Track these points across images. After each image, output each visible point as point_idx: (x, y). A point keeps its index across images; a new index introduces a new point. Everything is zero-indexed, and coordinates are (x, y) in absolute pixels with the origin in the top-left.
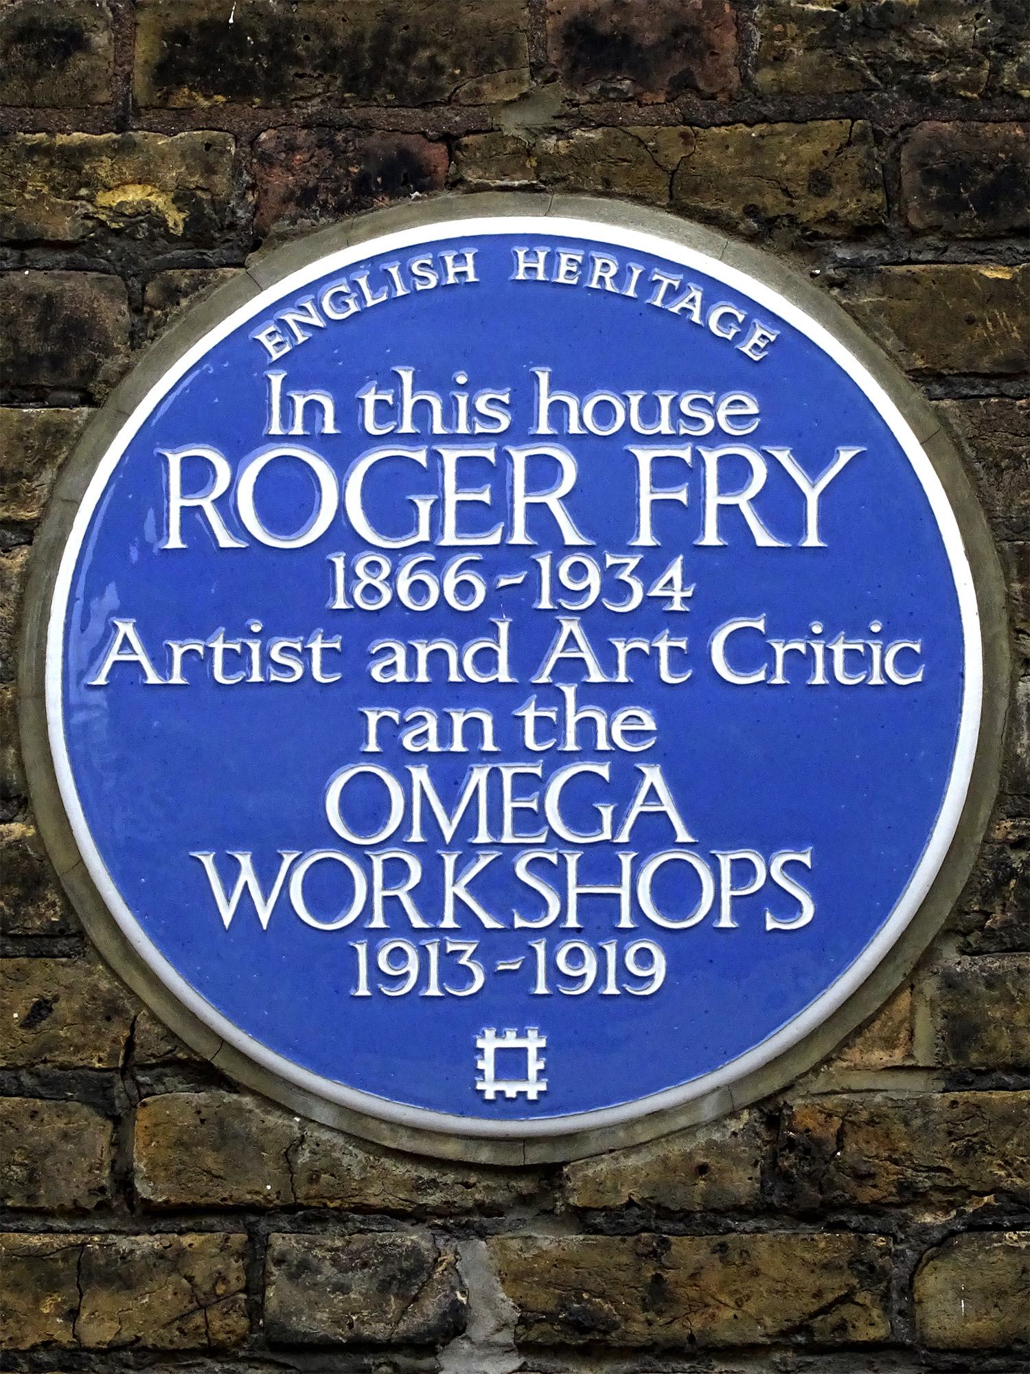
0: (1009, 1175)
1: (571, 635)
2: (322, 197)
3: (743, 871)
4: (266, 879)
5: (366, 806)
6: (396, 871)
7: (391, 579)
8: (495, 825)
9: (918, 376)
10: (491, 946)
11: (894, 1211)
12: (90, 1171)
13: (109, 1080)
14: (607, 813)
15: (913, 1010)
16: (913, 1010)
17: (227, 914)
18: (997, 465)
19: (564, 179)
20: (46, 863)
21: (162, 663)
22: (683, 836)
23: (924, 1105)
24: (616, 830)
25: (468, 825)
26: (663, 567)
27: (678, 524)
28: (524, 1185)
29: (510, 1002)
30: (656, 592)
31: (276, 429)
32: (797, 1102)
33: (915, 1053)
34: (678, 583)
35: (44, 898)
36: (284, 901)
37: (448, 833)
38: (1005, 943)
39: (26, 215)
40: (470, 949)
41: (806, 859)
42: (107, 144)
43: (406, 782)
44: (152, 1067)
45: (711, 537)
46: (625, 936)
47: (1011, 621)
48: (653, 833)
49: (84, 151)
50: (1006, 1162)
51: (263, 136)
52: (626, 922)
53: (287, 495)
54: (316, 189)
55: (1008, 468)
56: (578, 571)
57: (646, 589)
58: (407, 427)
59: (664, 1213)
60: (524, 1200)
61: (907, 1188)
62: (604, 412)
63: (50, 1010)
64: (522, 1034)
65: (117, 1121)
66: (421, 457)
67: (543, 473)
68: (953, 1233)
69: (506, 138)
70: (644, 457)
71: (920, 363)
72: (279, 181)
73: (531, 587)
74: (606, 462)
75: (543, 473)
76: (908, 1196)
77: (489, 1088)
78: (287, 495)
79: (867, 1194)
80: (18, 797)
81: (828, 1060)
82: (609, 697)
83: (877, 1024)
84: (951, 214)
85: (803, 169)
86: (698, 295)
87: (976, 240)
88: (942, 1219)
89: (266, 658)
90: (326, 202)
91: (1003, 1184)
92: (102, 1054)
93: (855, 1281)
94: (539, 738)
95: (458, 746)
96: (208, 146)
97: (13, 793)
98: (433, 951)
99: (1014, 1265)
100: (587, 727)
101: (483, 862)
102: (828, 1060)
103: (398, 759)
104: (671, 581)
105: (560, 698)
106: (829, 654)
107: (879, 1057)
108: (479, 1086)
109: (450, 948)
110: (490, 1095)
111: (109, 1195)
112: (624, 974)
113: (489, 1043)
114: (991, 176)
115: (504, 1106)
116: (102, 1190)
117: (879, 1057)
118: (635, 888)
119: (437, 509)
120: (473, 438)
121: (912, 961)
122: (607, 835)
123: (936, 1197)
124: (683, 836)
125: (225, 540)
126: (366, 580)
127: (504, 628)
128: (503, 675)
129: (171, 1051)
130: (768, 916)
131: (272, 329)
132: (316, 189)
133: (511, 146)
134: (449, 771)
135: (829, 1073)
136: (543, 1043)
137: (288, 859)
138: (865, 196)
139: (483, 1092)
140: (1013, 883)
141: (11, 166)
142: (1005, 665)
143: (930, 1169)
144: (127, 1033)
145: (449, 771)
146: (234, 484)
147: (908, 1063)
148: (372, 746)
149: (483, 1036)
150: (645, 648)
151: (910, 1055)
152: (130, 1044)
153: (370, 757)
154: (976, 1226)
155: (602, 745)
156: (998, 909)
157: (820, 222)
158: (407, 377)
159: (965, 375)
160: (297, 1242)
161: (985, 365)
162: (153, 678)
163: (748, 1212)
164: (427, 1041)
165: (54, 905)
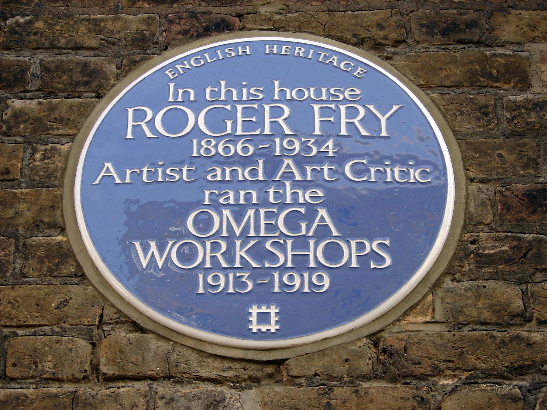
0: (480, 363)
1: (288, 164)
2: (191, 33)
3: (360, 247)
4: (161, 250)
5: (204, 223)
6: (215, 247)
7: (216, 146)
8: (257, 229)
9: (421, 86)
10: (255, 274)
11: (430, 379)
12: (81, 363)
13: (92, 329)
14: (303, 226)
15: (433, 301)
16: (433, 301)
17: (144, 264)
18: (455, 114)
19: (283, 27)
20: (71, 250)
21: (123, 176)
22: (335, 233)
23: (440, 335)
24: (308, 229)
25: (246, 229)
26: (325, 142)
27: (330, 129)
28: (269, 369)
29: (263, 295)
30: (322, 150)
31: (171, 99)
32: (385, 335)
33: (436, 317)
34: (331, 147)
35: (68, 263)
36: (169, 258)
37: (238, 233)
38: (471, 277)
39: (78, 39)
40: (246, 275)
41: (387, 243)
42: (111, 18)
43: (221, 215)
44: (110, 324)
45: (343, 132)
46: (312, 270)
47: (464, 166)
48: (323, 232)
49: (102, 20)
50: (478, 358)
51: (170, 15)
52: (312, 264)
53: (175, 120)
54: (189, 31)
55: (459, 115)
56: (291, 143)
57: (318, 149)
58: (223, 98)
59: (331, 377)
60: (270, 376)
61: (436, 369)
62: (300, 93)
63: (68, 303)
64: (268, 307)
65: (93, 345)
66: (228, 107)
67: (276, 112)
68: (457, 386)
69: (262, 15)
70: (316, 107)
71: (422, 82)
72: (176, 28)
73: (272, 148)
74: (302, 109)
75: (276, 112)
76: (437, 372)
77: (254, 328)
78: (175, 120)
79: (418, 370)
80: (61, 227)
81: (399, 320)
82: (304, 184)
83: (419, 307)
84: (431, 36)
85: (374, 23)
86: (336, 58)
87: (441, 45)
88: (450, 382)
89: (164, 173)
90: (193, 34)
91: (478, 366)
92: (89, 319)
93: (416, 404)
94: (275, 198)
95: (242, 202)
96: (149, 18)
97: (59, 226)
98: (231, 276)
99: (485, 397)
100: (295, 195)
101: (252, 243)
102: (399, 320)
103: (218, 208)
104: (328, 146)
105: (284, 186)
106: (392, 171)
107: (421, 319)
108: (250, 327)
109: (238, 275)
110: (255, 331)
111: (88, 373)
112: (311, 284)
113: (254, 310)
114: (446, 25)
115: (261, 335)
116: (86, 371)
117: (421, 319)
118: (316, 253)
119: (235, 123)
120: (248, 101)
121: (431, 284)
122: (304, 233)
123: (449, 372)
124: (335, 233)
125: (149, 135)
126: (206, 146)
127: (261, 162)
128: (261, 177)
129: (119, 318)
130: (372, 263)
131: (171, 69)
132: (189, 31)
133: (263, 17)
134: (239, 212)
135: (399, 325)
136: (277, 311)
137: (171, 243)
138: (398, 31)
139: (252, 329)
140: (472, 255)
141: (73, 25)
142: (463, 181)
143: (445, 361)
144: (100, 312)
145: (239, 212)
146: (153, 119)
147: (433, 321)
148: (207, 202)
149: (252, 308)
150: (318, 168)
151: (433, 317)
152: (101, 316)
153: (207, 206)
154: (468, 383)
155: (301, 201)
156: (467, 265)
157: (382, 39)
158: (223, 83)
159: (440, 86)
160: (170, 390)
161: (448, 83)
162: (118, 181)
163: (367, 378)
164: (228, 312)
165: (73, 265)
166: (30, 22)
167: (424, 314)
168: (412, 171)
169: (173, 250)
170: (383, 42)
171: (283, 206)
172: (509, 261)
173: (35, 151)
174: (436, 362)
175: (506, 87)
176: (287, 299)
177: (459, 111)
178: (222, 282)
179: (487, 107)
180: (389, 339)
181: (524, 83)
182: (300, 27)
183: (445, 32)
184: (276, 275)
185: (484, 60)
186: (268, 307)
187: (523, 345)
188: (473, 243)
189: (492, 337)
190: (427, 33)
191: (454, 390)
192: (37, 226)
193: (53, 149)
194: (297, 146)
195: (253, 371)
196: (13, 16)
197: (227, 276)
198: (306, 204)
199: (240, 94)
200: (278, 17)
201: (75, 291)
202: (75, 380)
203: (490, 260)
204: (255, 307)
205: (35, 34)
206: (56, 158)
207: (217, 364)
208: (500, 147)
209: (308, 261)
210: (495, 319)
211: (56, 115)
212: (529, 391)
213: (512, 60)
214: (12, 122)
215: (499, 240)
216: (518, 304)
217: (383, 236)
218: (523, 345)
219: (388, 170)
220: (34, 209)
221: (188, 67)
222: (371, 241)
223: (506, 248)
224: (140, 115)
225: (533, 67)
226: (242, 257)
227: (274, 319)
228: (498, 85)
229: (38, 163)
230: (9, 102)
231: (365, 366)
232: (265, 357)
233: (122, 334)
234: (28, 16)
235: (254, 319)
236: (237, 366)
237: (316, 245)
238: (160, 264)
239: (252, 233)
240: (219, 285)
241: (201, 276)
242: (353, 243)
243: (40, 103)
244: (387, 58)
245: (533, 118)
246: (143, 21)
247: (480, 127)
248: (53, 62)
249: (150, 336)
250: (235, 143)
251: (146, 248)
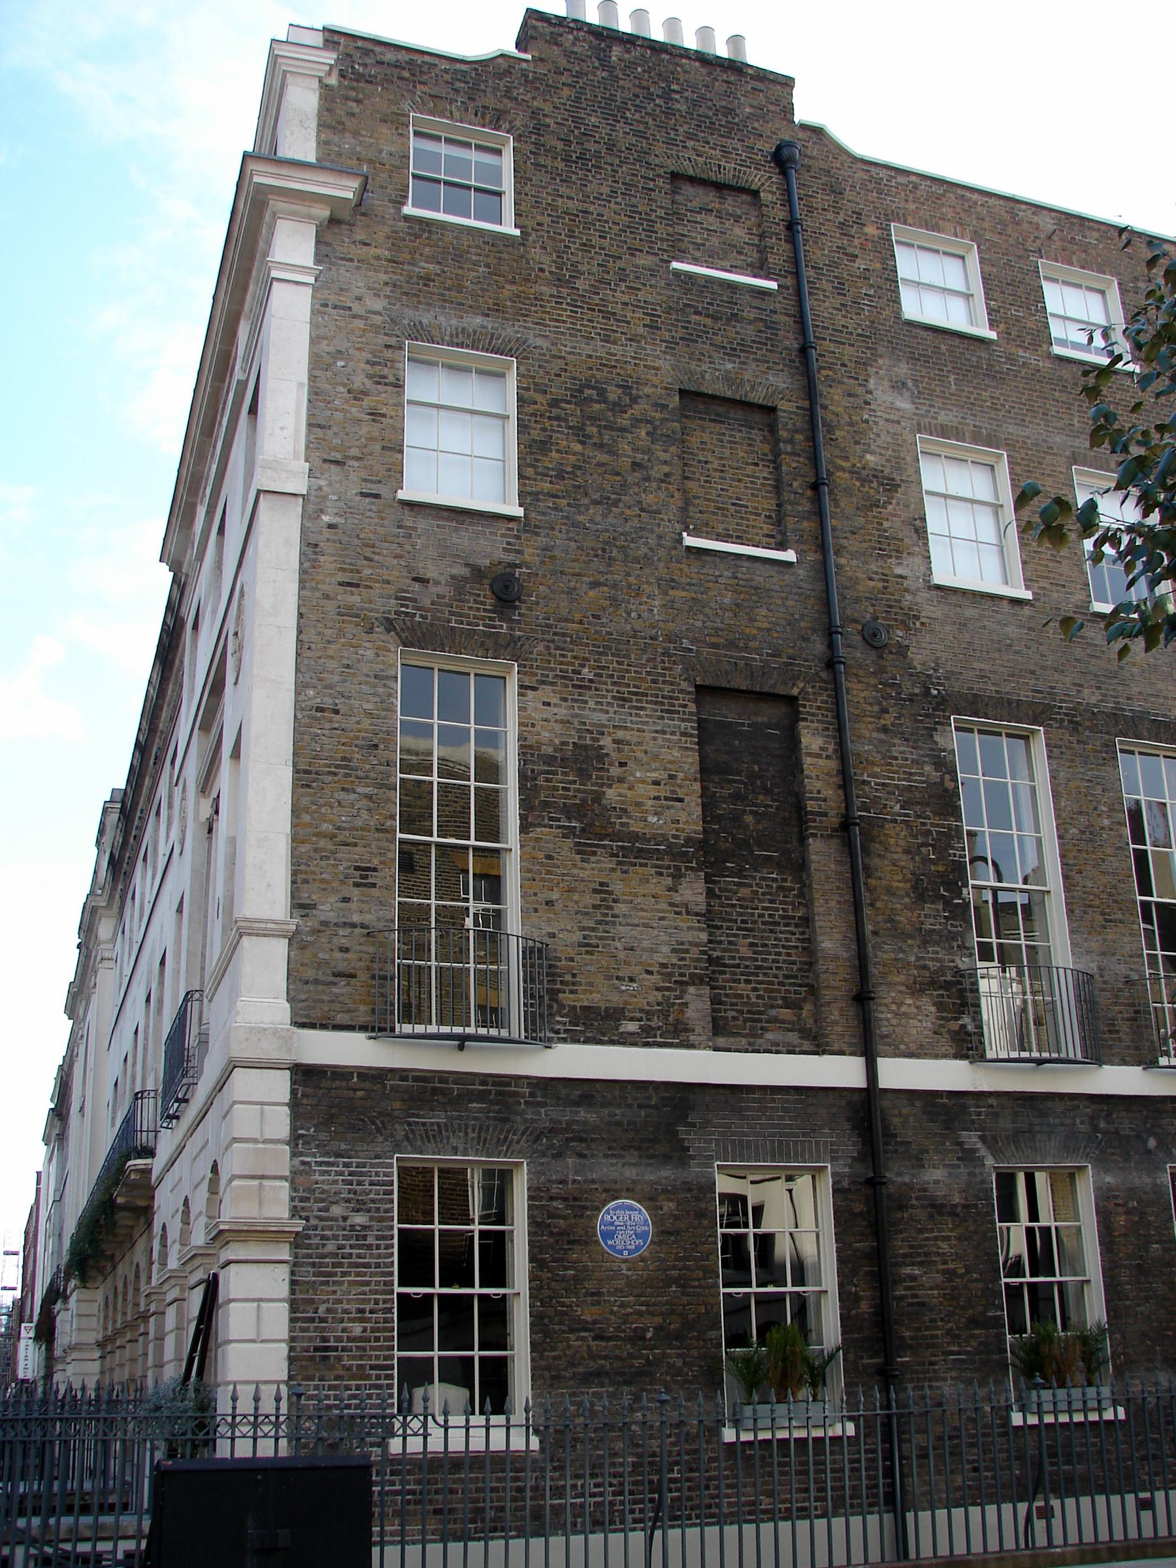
207: (150, 897)
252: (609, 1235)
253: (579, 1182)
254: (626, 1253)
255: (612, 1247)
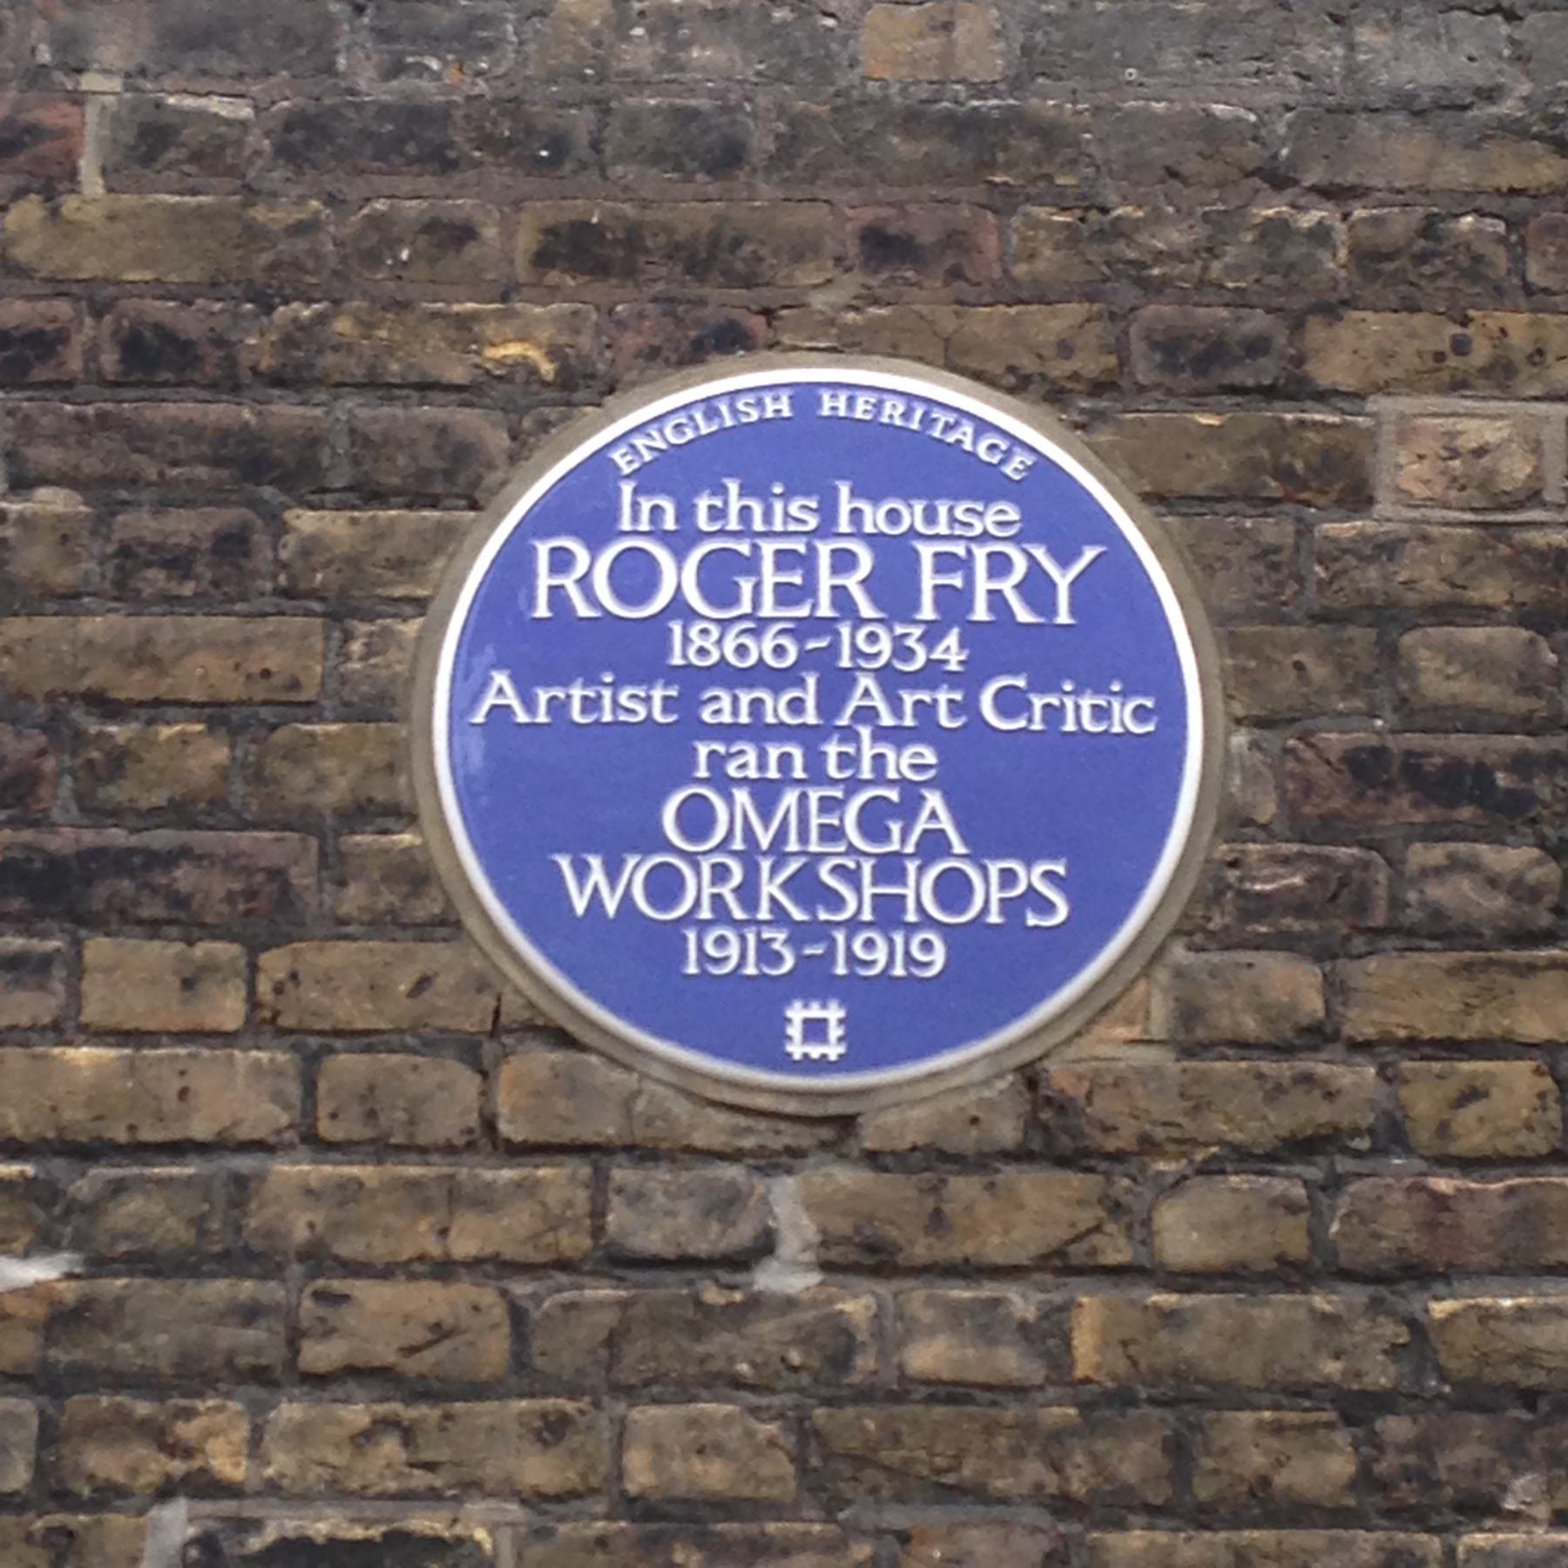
3: (1008, 878)
4: (612, 874)
5: (696, 820)
7: (719, 642)
8: (803, 837)
9: (1146, 498)
10: (799, 935)
14: (895, 828)
15: (1148, 995)
17: (580, 906)
22: (959, 847)
24: (903, 841)
25: (781, 836)
26: (942, 636)
27: (953, 603)
28: (826, 1133)
29: (813, 980)
31: (626, 525)
36: (627, 897)
37: (765, 841)
42: (495, 311)
43: (729, 800)
46: (911, 928)
48: (933, 846)
49: (474, 317)
52: (911, 917)
53: (635, 576)
56: (873, 638)
60: (824, 1145)
64: (824, 1006)
67: (843, 561)
70: (926, 552)
72: (630, 341)
73: (834, 649)
75: (843, 561)
78: (635, 576)
79: (1111, 1144)
81: (1078, 1034)
82: (897, 736)
94: (840, 768)
95: (773, 773)
102: (1078, 1034)
103: (724, 785)
106: (1078, 708)
107: (1122, 1032)
112: (909, 960)
113: (797, 1014)
117: (1122, 1032)
121: (1147, 956)
122: (895, 846)
123: (1171, 1147)
127: (811, 681)
128: (811, 718)
133: (819, 317)
134: (766, 794)
137: (631, 861)
142: (1221, 723)
145: (766, 794)
152: (497, 1013)
155: (892, 774)
166: (321, 319)
167: (1129, 1022)
168: (1116, 706)
169: (636, 870)
170: (1069, 385)
171: (853, 785)
172: (1302, 909)
173: (348, 637)
174: (1148, 1127)
175: (1322, 501)
176: (860, 992)
177: (1219, 558)
178: (734, 951)
179: (1277, 550)
180: (1059, 1076)
181: (1358, 499)
182: (895, 347)
183: (1202, 364)
184: (840, 937)
185: (1279, 435)
186: (824, 1006)
187: (1317, 1093)
188: (1233, 864)
189: (1260, 1076)
190: (1162, 367)
191: (1180, 1182)
192: (360, 813)
193: (386, 632)
194: (885, 646)
195: (790, 1136)
196: (286, 302)
197: (743, 939)
198: (902, 782)
199: (768, 516)
200: (851, 316)
201: (437, 956)
202: (449, 1149)
203: (1260, 906)
204: (798, 1005)
205: (336, 349)
206: (393, 654)
207: (722, 1118)
208: (1295, 646)
209: (903, 910)
210: (1266, 1037)
211: (385, 551)
212: (1323, 1189)
213: (1339, 436)
214: (299, 565)
215: (1286, 861)
216: (1313, 1004)
217: (1054, 857)
218: (1317, 1093)
219: (1069, 703)
220: (354, 771)
221: (663, 446)
222: (1029, 865)
223: (1297, 880)
224: (561, 561)
225: (1382, 455)
226: (773, 900)
227: (835, 1032)
228: (1305, 496)
229: (357, 666)
230: (289, 516)
231: (1007, 1132)
232: (816, 1110)
233: (540, 1060)
234: (318, 301)
235: (795, 1031)
236: (763, 1125)
237: (921, 870)
238: (611, 907)
239: (793, 846)
240: (726, 959)
241: (692, 936)
242: (994, 868)
243: (354, 522)
244: (1077, 426)
245: (1371, 576)
246: (556, 319)
247: (1261, 597)
248: (375, 420)
249: (593, 1059)
250: (756, 633)
251: (582, 871)
252: (564, 795)
253: (214, 153)
254: (814, 1030)
255: (634, 954)
